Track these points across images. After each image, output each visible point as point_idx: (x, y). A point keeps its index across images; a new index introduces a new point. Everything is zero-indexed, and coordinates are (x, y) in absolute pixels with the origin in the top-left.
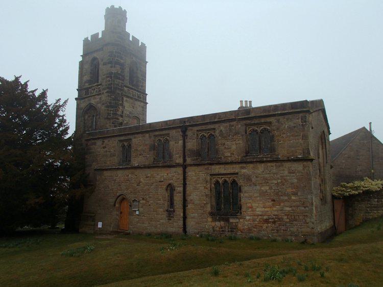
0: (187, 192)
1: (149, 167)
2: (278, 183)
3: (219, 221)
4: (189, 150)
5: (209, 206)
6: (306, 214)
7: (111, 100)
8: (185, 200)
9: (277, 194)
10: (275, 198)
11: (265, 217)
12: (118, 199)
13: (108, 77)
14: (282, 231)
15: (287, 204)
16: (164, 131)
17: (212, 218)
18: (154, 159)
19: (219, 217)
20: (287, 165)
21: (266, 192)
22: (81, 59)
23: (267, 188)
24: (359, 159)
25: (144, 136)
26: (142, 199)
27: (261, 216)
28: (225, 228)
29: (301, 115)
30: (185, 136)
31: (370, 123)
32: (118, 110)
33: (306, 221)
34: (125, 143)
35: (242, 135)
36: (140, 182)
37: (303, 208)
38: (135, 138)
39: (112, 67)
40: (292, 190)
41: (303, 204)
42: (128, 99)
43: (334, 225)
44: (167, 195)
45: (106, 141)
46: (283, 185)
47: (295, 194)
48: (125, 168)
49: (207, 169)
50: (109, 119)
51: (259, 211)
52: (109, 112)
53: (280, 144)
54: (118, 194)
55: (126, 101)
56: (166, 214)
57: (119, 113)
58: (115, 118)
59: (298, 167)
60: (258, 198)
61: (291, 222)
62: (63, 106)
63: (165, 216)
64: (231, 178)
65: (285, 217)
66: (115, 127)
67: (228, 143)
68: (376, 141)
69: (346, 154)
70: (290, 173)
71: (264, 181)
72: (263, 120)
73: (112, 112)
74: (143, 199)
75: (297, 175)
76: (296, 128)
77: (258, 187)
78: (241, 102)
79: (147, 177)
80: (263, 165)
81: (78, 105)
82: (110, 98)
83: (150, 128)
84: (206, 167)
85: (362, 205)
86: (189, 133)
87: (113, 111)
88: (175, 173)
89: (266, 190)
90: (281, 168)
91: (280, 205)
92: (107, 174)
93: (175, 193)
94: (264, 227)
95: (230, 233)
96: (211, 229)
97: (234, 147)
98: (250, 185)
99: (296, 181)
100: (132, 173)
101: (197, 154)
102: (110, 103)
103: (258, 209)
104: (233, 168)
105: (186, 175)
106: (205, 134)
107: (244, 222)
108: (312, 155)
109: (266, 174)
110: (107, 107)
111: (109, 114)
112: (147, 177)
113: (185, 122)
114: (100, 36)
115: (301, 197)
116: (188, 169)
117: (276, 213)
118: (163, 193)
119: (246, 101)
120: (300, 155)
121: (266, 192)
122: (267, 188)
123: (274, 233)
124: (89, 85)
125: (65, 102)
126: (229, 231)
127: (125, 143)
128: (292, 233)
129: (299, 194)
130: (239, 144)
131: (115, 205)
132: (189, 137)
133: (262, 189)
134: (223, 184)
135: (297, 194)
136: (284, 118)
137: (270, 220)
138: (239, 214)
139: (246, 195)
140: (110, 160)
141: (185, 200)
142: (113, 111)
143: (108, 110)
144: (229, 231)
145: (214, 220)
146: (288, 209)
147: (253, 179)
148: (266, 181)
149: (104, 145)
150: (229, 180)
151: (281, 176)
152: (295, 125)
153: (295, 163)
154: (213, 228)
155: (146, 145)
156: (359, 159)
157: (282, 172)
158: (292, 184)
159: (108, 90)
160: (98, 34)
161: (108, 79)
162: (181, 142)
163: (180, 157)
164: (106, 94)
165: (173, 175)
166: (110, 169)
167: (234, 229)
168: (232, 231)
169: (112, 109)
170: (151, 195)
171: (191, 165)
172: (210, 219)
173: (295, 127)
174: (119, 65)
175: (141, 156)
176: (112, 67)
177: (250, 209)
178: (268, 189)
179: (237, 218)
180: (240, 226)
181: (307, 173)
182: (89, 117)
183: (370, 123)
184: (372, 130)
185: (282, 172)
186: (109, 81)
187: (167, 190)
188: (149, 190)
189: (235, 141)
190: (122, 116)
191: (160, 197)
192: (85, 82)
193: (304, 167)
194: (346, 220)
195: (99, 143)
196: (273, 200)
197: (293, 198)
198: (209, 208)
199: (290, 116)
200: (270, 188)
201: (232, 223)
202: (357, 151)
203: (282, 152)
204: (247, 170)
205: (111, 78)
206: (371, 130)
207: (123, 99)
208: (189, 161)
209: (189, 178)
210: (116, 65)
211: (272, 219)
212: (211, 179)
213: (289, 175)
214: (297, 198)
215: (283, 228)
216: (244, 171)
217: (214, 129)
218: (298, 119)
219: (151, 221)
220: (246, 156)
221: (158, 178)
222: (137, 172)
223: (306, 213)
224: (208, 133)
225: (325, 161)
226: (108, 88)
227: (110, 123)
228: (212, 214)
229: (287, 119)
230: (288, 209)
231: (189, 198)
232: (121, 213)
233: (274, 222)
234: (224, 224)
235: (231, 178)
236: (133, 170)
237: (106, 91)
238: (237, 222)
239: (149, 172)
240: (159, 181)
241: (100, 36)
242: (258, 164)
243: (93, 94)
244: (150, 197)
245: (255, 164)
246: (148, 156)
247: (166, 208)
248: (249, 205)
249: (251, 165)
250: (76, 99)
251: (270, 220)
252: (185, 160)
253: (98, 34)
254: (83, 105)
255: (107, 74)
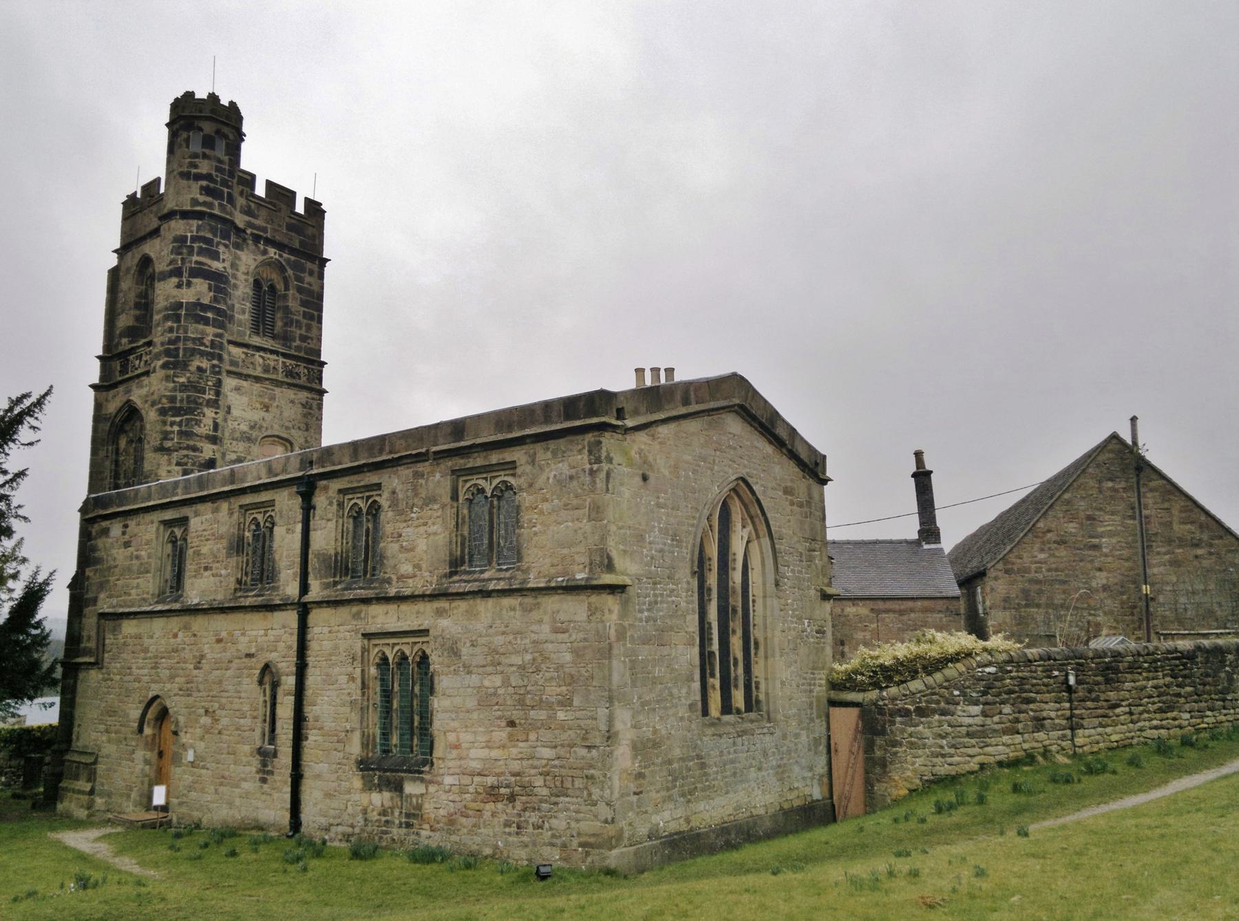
0: (309, 693)
1: (222, 610)
2: (522, 667)
3: (379, 789)
4: (317, 556)
5: (356, 738)
6: (592, 771)
7: (174, 389)
8: (299, 719)
9: (521, 702)
10: (516, 715)
11: (490, 780)
12: (152, 709)
14: (530, 829)
15: (546, 735)
16: (263, 494)
17: (363, 777)
18: (239, 582)
19: (380, 777)
20: (551, 603)
21: (495, 694)
22: (113, 261)
23: (497, 680)
24: (1096, 547)
26: (202, 711)
27: (479, 774)
28: (392, 813)
29: (589, 437)
30: (308, 509)
31: (1134, 420)
32: (198, 423)
33: (590, 794)
34: (176, 530)
35: (443, 506)
36: (202, 657)
37: (584, 752)
38: (197, 514)
39: (179, 286)
40: (558, 690)
41: (584, 739)
42: (245, 383)
43: (831, 797)
44: (262, 699)
45: (132, 523)
46: (538, 671)
47: (566, 703)
48: (169, 611)
49: (357, 616)
50: (168, 451)
51: (477, 756)
52: (168, 428)
53: (536, 534)
54: (151, 695)
55: (237, 389)
56: (256, 762)
57: (205, 428)
58: (188, 448)
59: (574, 609)
60: (475, 716)
61: (553, 799)
62: (29, 412)
63: (254, 770)
64: (416, 648)
65: (539, 781)
66: (185, 473)
67: (408, 532)
68: (818, 524)
69: (1049, 531)
70: (556, 631)
71: (489, 658)
72: (495, 458)
73: (176, 428)
75: (574, 637)
76: (575, 483)
77: (474, 679)
78: (640, 372)
79: (219, 641)
80: (490, 602)
81: (98, 406)
82: (171, 385)
83: (232, 483)
84: (355, 609)
85: (920, 728)
86: (320, 500)
87: (180, 424)
88: (284, 627)
89: (496, 689)
90: (535, 615)
91: (527, 741)
92: (129, 627)
93: (280, 691)
94: (487, 815)
95: (404, 830)
96: (360, 818)
97: (422, 545)
98: (456, 672)
99: (568, 657)
100: (186, 627)
101: (340, 567)
102: (172, 399)
103: (473, 753)
104: (418, 612)
105: (309, 637)
106: (480, 482)
107: (439, 795)
108: (627, 569)
109: (497, 634)
110: (163, 412)
111: (166, 436)
112: (219, 641)
114: (139, 196)
115: (579, 714)
117: (516, 766)
118: (252, 693)
119: (655, 371)
120: (581, 572)
121: (495, 694)
122: (497, 680)
123: (509, 834)
124: (130, 342)
125: (39, 403)
126: (400, 826)
127: (176, 530)
128: (553, 836)
129: (576, 702)
130: (435, 534)
131: (141, 730)
132: (318, 512)
133: (486, 683)
134: (399, 664)
135: (571, 705)
136: (548, 449)
137: (502, 791)
138: (427, 768)
139: (446, 703)
140: (138, 587)
141: (299, 719)
142: (180, 424)
143: (165, 423)
144: (400, 826)
145: (369, 786)
146: (547, 753)
147: (464, 651)
148: (495, 659)
150: (408, 648)
151: (534, 642)
152: (573, 472)
153: (569, 598)
154: (365, 812)
155: (221, 537)
156: (1096, 547)
157: (534, 628)
158: (559, 667)
160: (135, 193)
161: (169, 324)
164: (161, 373)
165: (273, 635)
166: (135, 614)
167: (413, 817)
168: (409, 825)
169: (178, 419)
170: (224, 701)
171: (319, 604)
172: (358, 783)
173: (571, 478)
174: (205, 278)
175: (206, 574)
176: (179, 286)
177: (455, 753)
178: (499, 684)
179: (422, 780)
180: (428, 807)
181: (598, 632)
182: (130, 442)
183: (1134, 420)
184: (1140, 444)
185: (534, 628)
186: (171, 330)
187: (261, 682)
188: (220, 682)
189: (425, 524)
190: (214, 440)
191: (246, 708)
192: (122, 335)
193: (592, 611)
194: (869, 784)
195: (116, 529)
196: (512, 724)
197: (561, 715)
198: (355, 749)
199: (562, 443)
200: (506, 683)
201: (410, 796)
202: (1089, 518)
203: (539, 564)
204: (448, 622)
205: (177, 318)
206: (1135, 443)
207: (219, 383)
208: (316, 591)
209: (314, 647)
210: (194, 280)
211: (507, 786)
212: (365, 650)
213: (553, 637)
214: (570, 716)
215: (533, 818)
216: (444, 623)
217: (378, 486)
218: (580, 452)
219: (221, 784)
220: (452, 574)
221: (243, 645)
222: (199, 623)
223: (591, 766)
224: (368, 498)
225: (771, 577)
226: (167, 353)
227: (169, 463)
228: (364, 765)
229: (554, 454)
230: (547, 753)
231: (310, 711)
232: (161, 754)
233: (512, 798)
234: (392, 798)
235: (397, 648)
236: (186, 619)
237: (160, 363)
238: (422, 795)
239: (221, 624)
241: (139, 196)
242: (478, 601)
243: (139, 371)
244: (222, 707)
245: (471, 602)
247: (258, 744)
248: (452, 737)
249: (462, 605)
250: (93, 386)
251: (502, 791)
252: (304, 588)
253: (135, 193)
254: (112, 407)
255: (166, 309)
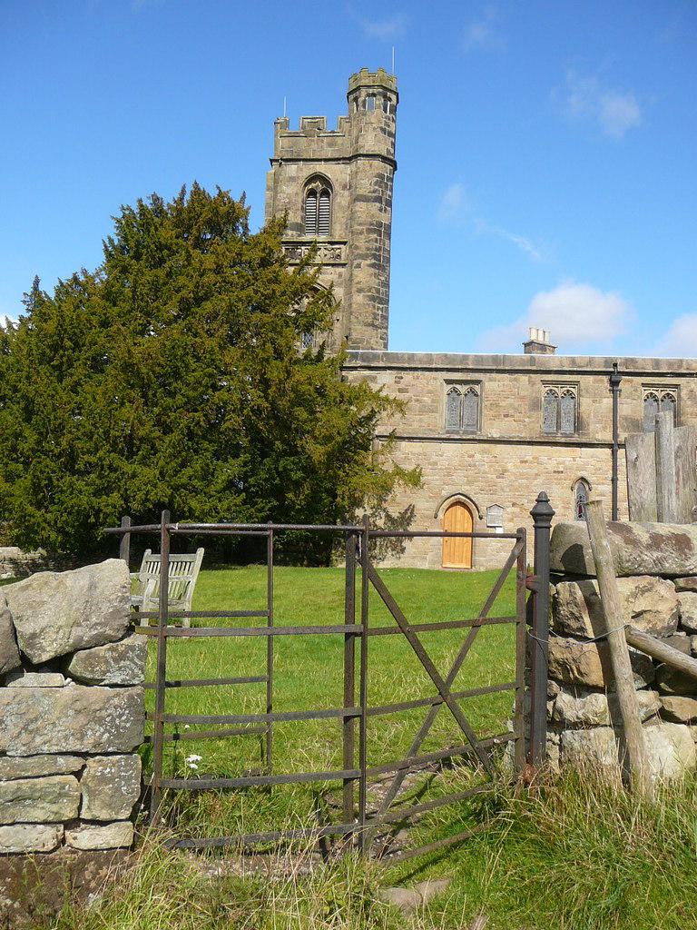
4: (626, 419)
13: (369, 231)
25: (515, 380)
36: (506, 471)
74: (514, 505)
100: (484, 452)
113: (615, 365)
116: (608, 451)
149: (400, 386)
155: (523, 398)
159: (373, 261)
162: (608, 402)
163: (604, 428)
169: (381, 306)
217: (677, 386)
221: (551, 466)
226: (374, 256)
237: (368, 262)
240: (555, 472)
246: (527, 420)
